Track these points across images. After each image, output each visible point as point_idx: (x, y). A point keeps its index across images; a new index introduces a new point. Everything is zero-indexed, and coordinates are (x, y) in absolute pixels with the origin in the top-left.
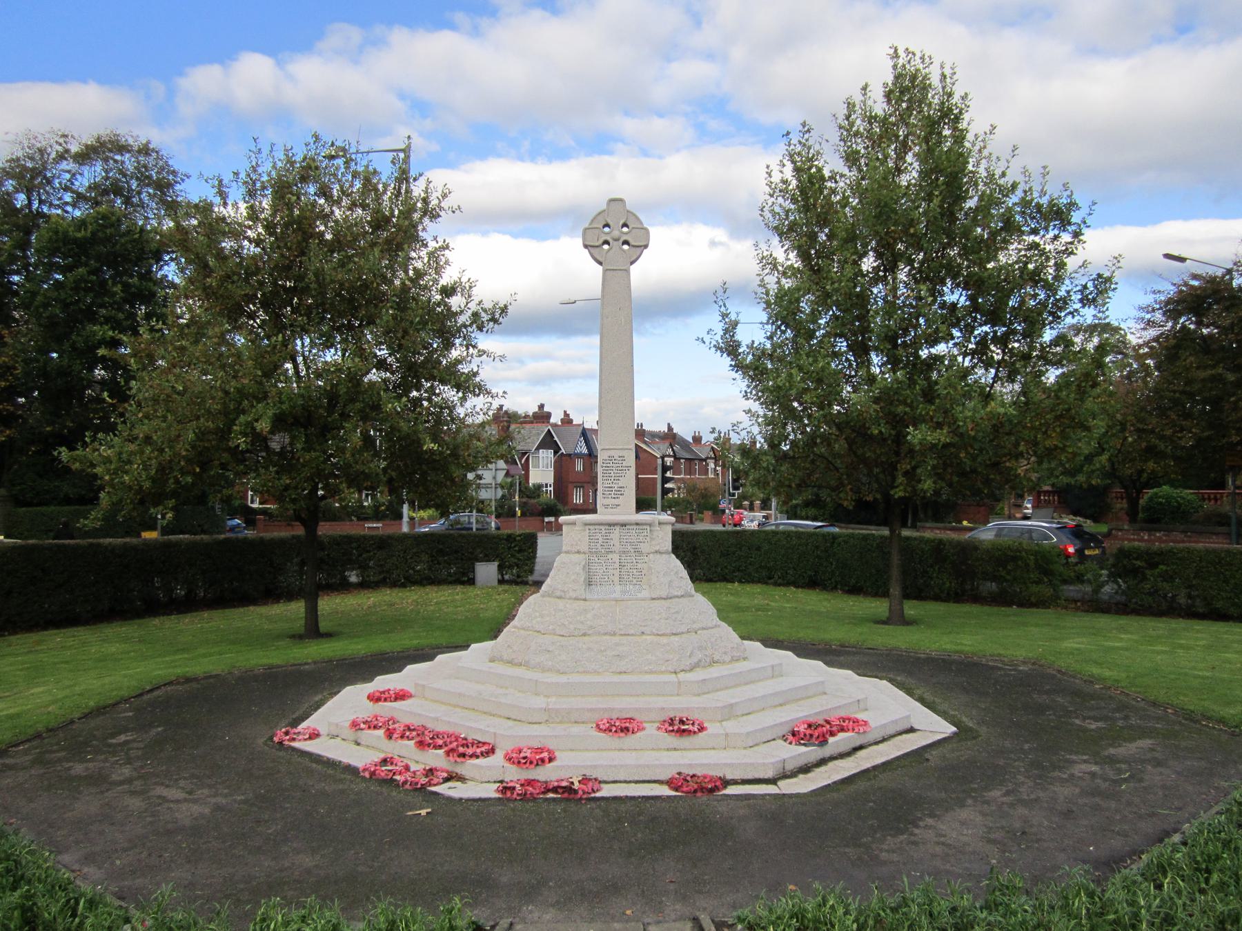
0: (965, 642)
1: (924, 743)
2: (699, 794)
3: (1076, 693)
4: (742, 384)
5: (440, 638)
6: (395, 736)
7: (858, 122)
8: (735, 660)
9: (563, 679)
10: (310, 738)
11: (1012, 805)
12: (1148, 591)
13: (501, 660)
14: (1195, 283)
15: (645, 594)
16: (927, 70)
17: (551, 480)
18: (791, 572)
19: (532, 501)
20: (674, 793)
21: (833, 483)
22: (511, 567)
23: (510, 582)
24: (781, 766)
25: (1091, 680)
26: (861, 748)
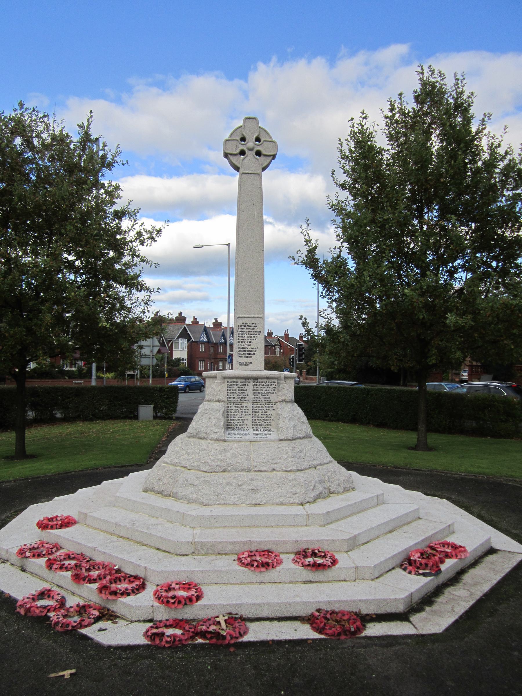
2: (343, 637)
6: (55, 566)
8: (346, 490)
9: (206, 511)
13: (153, 490)
15: (274, 436)
19: (175, 368)
20: (316, 636)
22: (161, 408)
23: (161, 418)
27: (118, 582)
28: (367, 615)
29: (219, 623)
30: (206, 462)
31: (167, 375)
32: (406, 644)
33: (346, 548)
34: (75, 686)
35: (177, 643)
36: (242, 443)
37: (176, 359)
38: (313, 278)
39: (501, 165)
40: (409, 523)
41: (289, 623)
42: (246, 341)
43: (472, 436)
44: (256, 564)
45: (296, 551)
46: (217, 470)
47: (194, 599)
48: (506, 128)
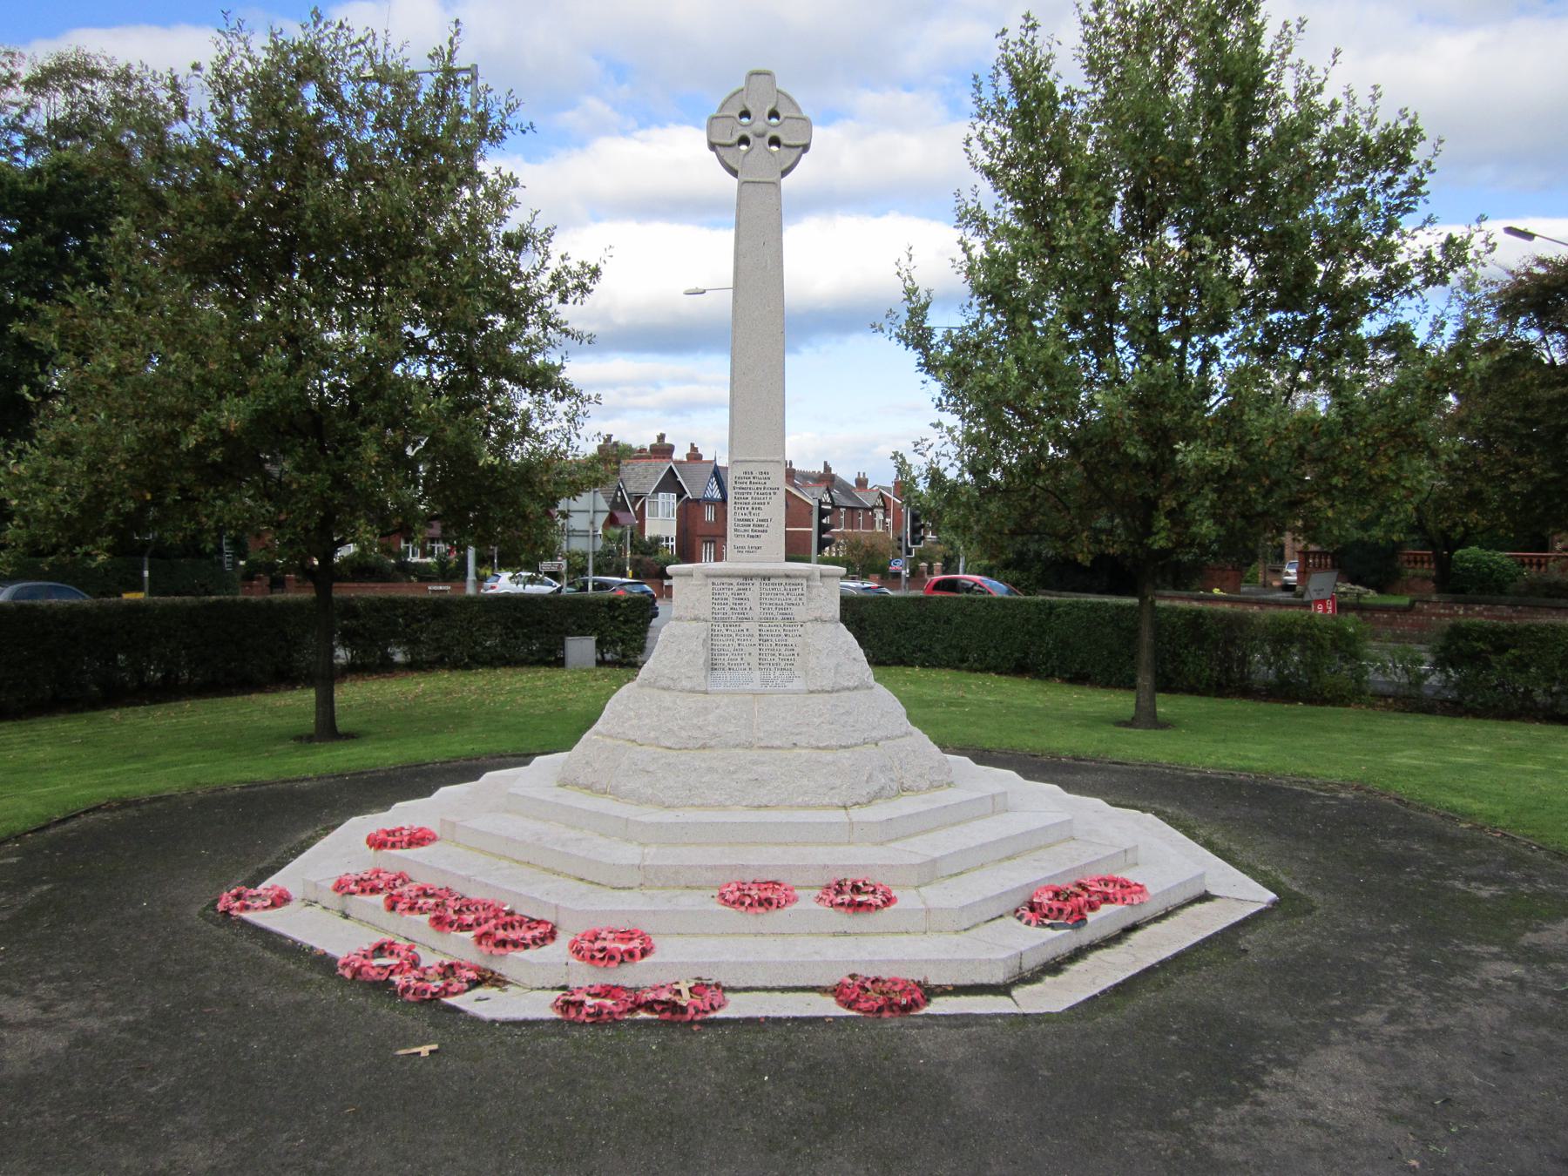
2: (886, 1015)
3: (1439, 838)
5: (506, 743)
6: (401, 906)
7: (1109, 18)
8: (934, 786)
9: (668, 817)
10: (274, 905)
11: (1407, 1042)
12: (1493, 682)
14: (1540, 271)
15: (797, 684)
17: (673, 534)
18: (992, 653)
19: (648, 559)
21: (1062, 528)
22: (613, 643)
23: (612, 664)
25: (1453, 815)
26: (1134, 928)
29: (679, 992)
34: (437, 1065)
36: (738, 698)
39: (1324, 130)
40: (1050, 845)
44: (748, 901)
47: (638, 953)
48: (1337, 53)
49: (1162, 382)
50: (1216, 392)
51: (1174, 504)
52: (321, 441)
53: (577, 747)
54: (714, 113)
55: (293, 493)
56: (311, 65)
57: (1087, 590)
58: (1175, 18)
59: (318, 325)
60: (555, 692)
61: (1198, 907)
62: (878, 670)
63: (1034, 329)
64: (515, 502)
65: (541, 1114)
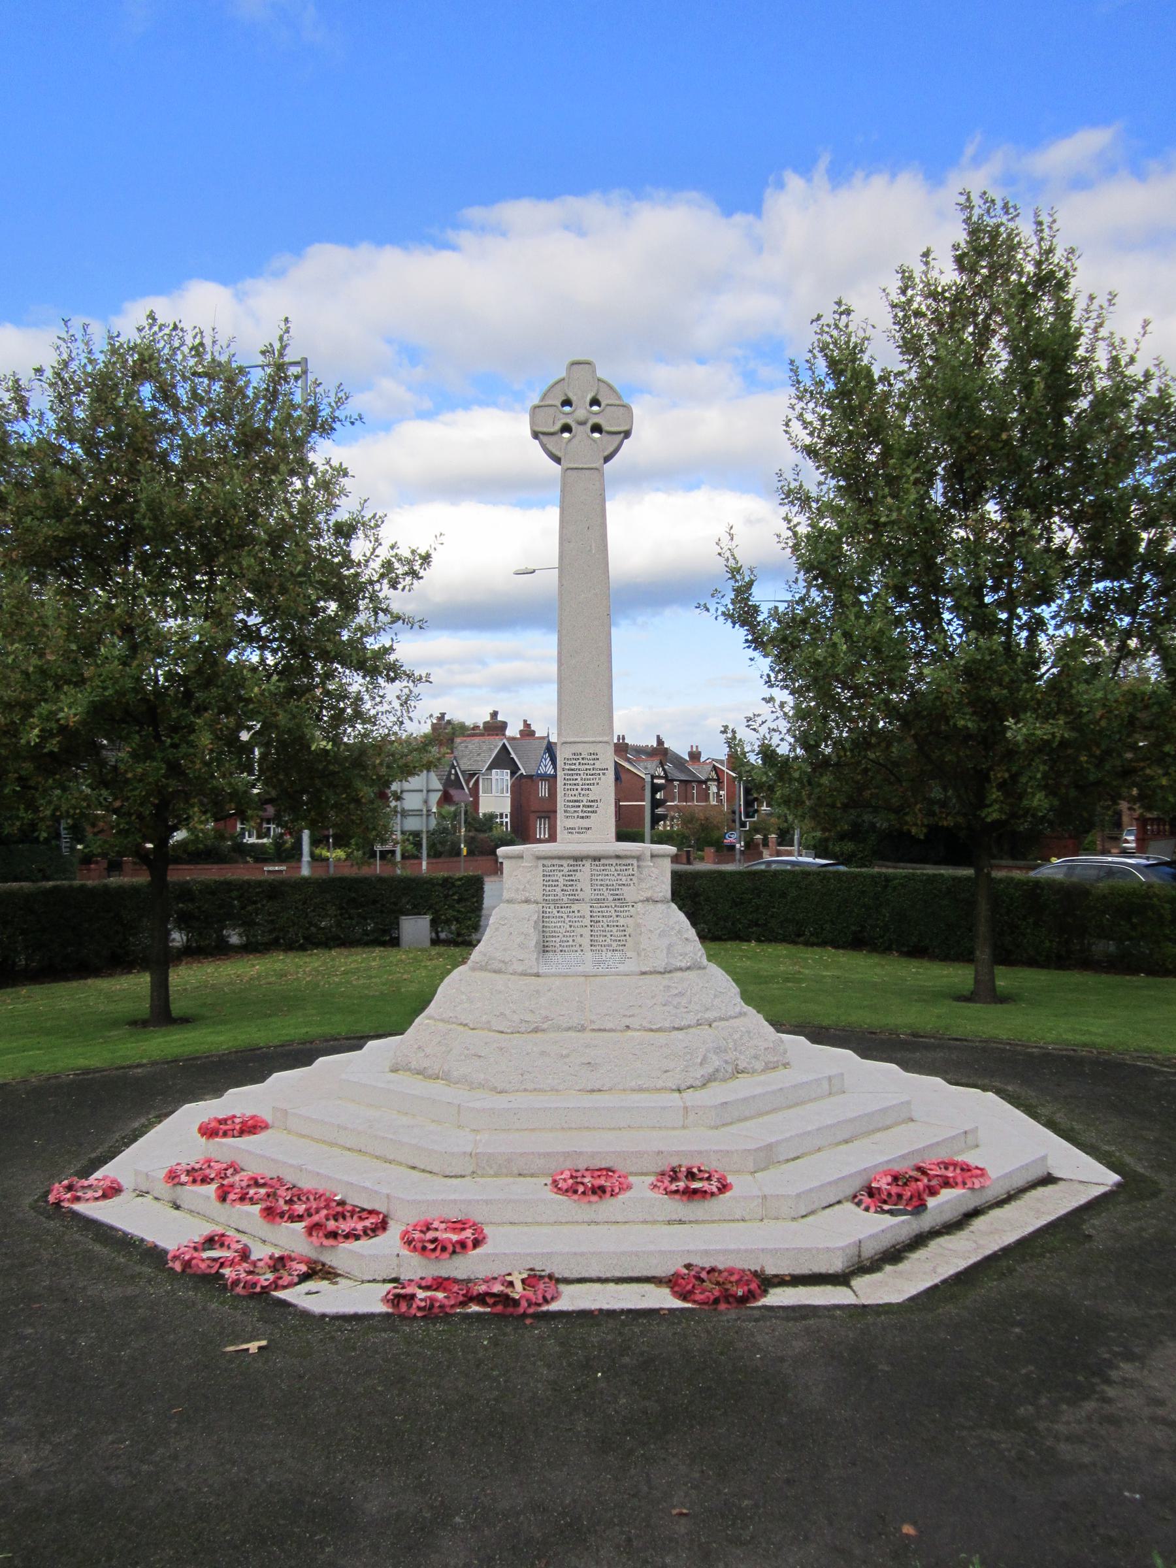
0: (1094, 1029)
1: (1082, 1200)
2: (722, 1306)
4: (764, 664)
5: (340, 1026)
6: (232, 1196)
8: (770, 1067)
10: (105, 1196)
15: (630, 966)
16: (1011, 225)
17: (507, 810)
18: (827, 926)
19: (482, 836)
20: (679, 1304)
21: (895, 802)
22: (448, 922)
23: (448, 943)
24: (855, 1251)
26: (976, 1213)
27: (341, 1220)
28: (776, 1276)
29: (511, 1284)
30: (502, 1014)
31: (465, 852)
32: (833, 1317)
33: (751, 1166)
35: (436, 1310)
36: (570, 980)
37: (484, 815)
38: (749, 647)
40: (888, 1128)
41: (634, 1286)
42: (579, 788)
43: (1107, 973)
44: (581, 1189)
45: (659, 1170)
46: (523, 1029)
47: (470, 1244)
48: (1146, 323)
49: (988, 658)
50: (1045, 662)
51: (1006, 775)
52: (156, 730)
53: (411, 1031)
54: (536, 402)
55: (127, 781)
56: (146, 365)
57: (924, 860)
58: (986, 296)
59: (153, 614)
60: (390, 973)
61: (1041, 1190)
62: (712, 945)
63: (861, 603)
64: (348, 786)
65: (369, 1414)
